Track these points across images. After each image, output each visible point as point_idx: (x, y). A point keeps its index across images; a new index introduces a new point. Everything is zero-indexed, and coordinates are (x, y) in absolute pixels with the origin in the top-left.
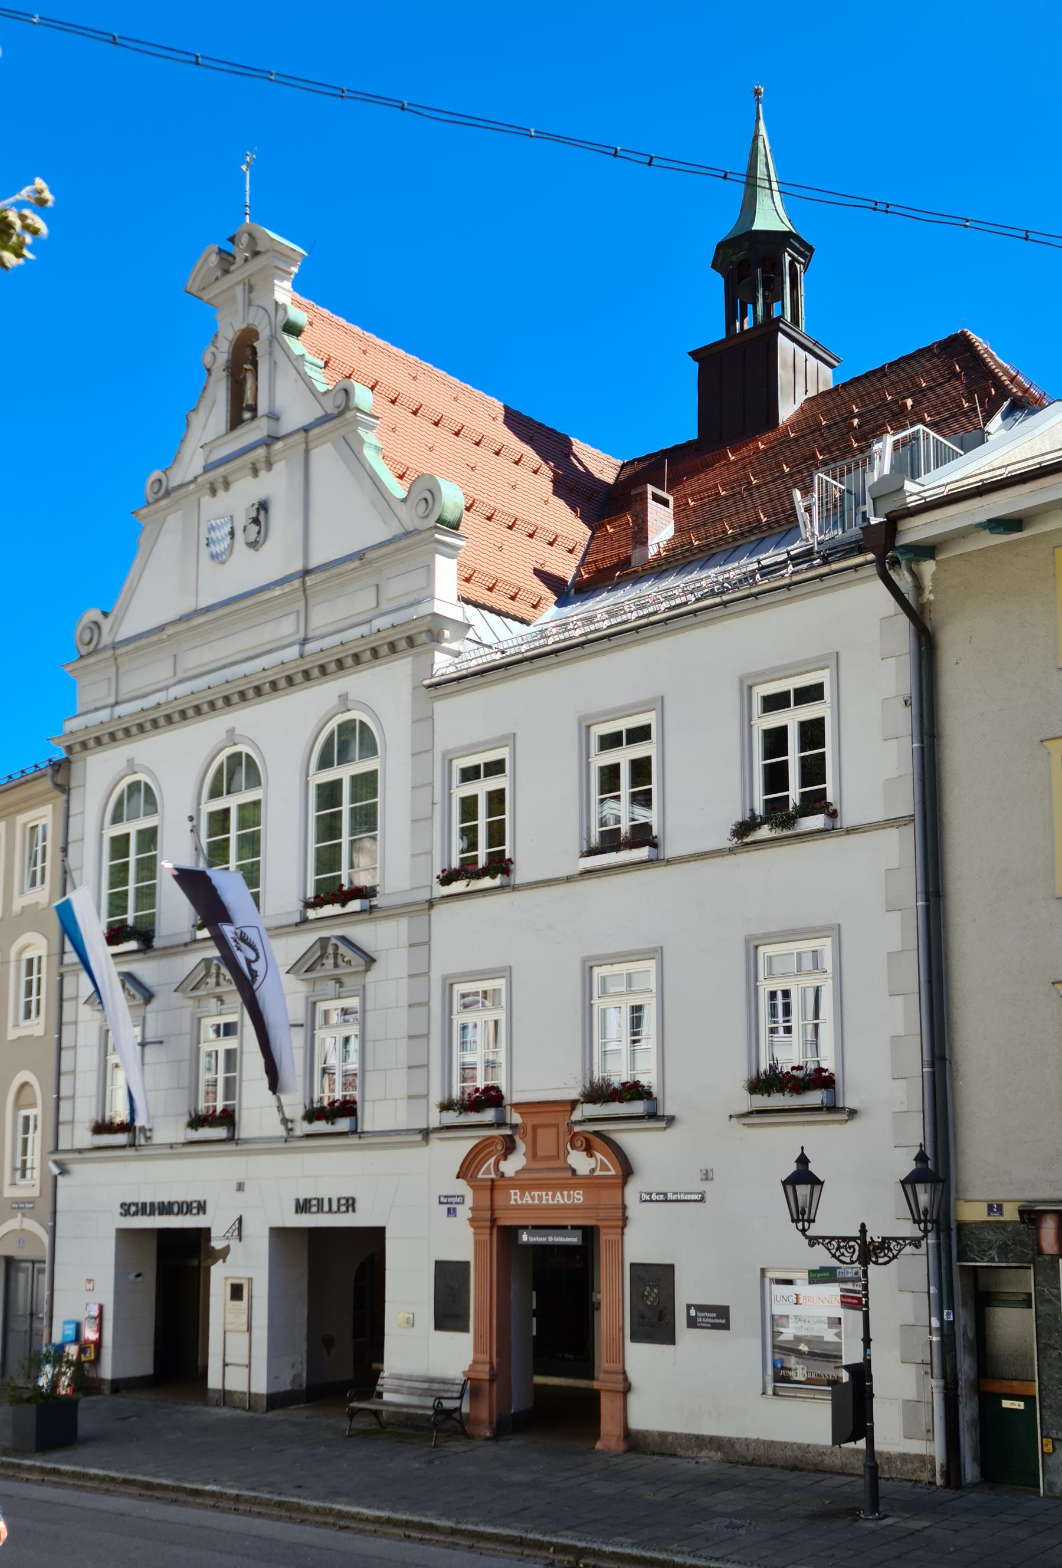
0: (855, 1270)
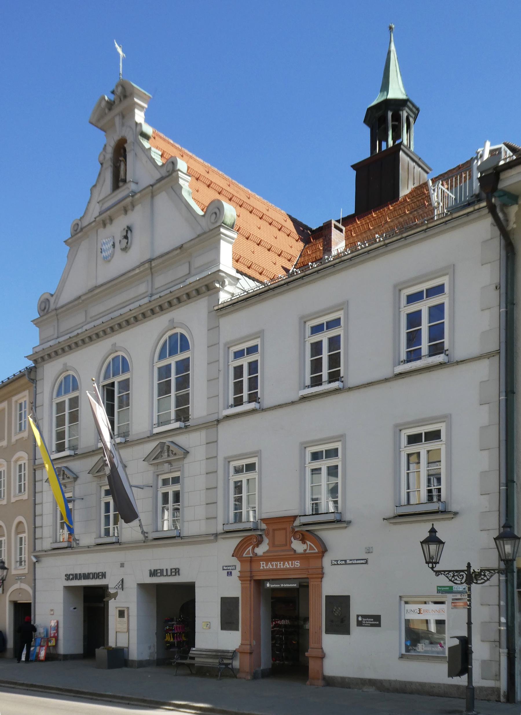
0: (464, 587)
